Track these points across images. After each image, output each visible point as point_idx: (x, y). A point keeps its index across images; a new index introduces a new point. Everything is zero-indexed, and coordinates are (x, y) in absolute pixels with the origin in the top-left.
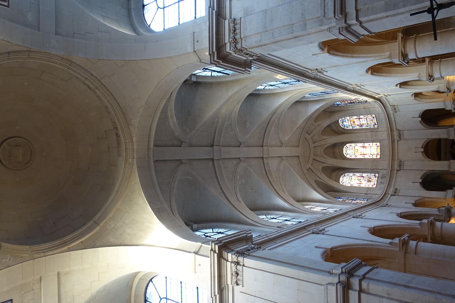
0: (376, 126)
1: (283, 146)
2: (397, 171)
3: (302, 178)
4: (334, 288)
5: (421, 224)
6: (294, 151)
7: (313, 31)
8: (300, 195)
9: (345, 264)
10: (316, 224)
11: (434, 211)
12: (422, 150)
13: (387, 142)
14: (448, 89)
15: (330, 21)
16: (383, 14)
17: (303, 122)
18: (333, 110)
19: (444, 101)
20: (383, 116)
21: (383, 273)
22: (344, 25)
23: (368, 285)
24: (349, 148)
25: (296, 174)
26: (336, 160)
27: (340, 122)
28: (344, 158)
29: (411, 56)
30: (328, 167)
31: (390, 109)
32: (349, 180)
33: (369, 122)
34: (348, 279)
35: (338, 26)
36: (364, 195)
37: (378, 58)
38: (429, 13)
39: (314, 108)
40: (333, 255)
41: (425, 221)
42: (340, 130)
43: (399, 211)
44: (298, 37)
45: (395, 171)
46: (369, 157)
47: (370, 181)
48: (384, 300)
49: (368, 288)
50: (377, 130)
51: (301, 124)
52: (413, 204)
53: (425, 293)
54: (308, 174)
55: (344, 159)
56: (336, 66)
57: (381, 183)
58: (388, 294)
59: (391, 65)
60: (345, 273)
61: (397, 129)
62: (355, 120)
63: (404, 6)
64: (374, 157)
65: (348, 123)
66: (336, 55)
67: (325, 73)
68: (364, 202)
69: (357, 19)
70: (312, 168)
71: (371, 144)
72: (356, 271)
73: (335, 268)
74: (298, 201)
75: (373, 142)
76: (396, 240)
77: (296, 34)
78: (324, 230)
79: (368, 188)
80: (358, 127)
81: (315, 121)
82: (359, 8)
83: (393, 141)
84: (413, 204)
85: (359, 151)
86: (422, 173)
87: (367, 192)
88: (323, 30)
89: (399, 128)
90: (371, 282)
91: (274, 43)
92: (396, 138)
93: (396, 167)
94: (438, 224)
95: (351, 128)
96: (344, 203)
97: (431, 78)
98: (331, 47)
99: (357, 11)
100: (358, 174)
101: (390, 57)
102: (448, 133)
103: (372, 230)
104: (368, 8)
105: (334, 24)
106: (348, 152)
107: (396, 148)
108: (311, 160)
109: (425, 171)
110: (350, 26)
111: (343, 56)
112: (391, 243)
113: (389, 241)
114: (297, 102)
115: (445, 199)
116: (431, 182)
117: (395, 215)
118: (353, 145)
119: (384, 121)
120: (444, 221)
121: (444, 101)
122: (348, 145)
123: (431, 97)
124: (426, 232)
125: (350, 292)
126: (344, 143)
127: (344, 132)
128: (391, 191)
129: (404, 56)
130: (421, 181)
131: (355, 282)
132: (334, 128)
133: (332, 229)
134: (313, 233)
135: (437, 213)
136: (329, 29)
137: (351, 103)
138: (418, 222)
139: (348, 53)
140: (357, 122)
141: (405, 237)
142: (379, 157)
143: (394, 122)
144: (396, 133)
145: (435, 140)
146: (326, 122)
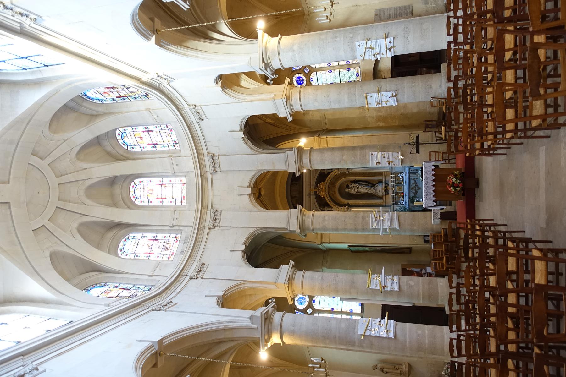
2: (210, 229)
12: (249, 191)
13: (194, 176)
19: (273, 99)
24: (138, 187)
26: (116, 210)
28: (130, 204)
29: (502, 234)
31: (188, 111)
32: (135, 246)
33: (165, 139)
36: (146, 277)
42: (121, 152)
45: (206, 229)
46: (170, 204)
47: (167, 249)
50: (178, 155)
55: (129, 208)
61: (208, 153)
64: (179, 204)
71: (173, 179)
75: (174, 174)
78: (37, 369)
83: (203, 176)
89: (212, 150)
92: (209, 168)
93: (208, 222)
95: (137, 149)
100: (150, 235)
102: (287, 160)
106: (138, 194)
108: (50, 211)
109: (252, 230)
112: (251, 318)
116: (263, 251)
118: (145, 180)
122: (137, 181)
127: (125, 156)
128: (191, 271)
130: (243, 248)
144: (207, 160)
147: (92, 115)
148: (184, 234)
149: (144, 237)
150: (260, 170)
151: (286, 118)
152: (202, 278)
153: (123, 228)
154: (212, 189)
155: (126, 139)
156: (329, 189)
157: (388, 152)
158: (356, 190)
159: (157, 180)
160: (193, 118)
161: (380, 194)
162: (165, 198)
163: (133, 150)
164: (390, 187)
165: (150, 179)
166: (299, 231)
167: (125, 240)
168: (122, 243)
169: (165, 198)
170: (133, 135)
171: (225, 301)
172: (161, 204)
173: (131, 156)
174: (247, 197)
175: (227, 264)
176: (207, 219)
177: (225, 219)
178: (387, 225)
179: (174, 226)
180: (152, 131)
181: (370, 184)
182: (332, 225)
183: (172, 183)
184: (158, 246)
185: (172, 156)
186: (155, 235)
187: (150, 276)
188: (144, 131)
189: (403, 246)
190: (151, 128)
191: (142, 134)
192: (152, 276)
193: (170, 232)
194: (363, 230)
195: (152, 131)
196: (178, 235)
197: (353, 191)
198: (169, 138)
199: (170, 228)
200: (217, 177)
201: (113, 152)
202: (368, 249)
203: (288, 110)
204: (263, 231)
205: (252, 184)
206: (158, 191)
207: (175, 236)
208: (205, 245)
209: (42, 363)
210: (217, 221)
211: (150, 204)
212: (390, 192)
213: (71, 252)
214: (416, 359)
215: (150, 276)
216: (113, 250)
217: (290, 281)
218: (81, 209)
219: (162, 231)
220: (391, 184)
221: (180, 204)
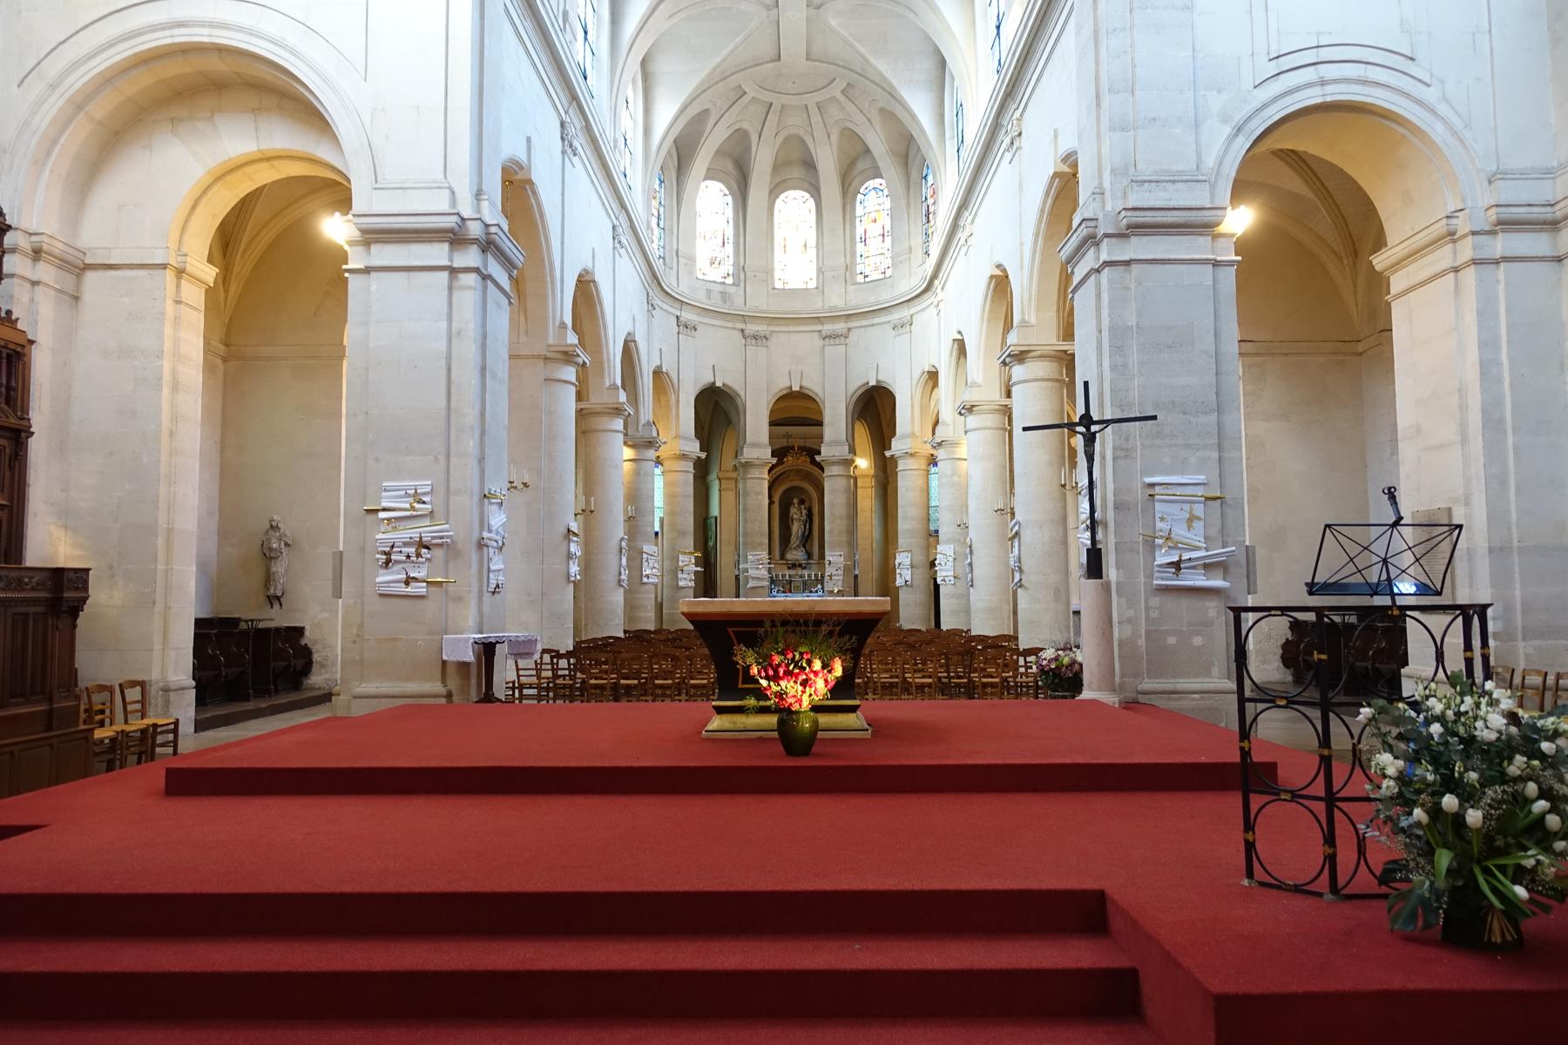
0: (860, 279)
1: (813, 11)
3: (714, 70)
4: (444, 206)
5: (614, 387)
6: (793, 48)
7: (1105, 149)
8: (663, 67)
9: (506, 228)
10: (588, 128)
11: (647, 412)
12: (796, 388)
13: (817, 306)
14: (940, 444)
15: (1120, 194)
16: (1105, 323)
17: (881, 74)
18: (910, 159)
19: (912, 435)
20: (885, 297)
21: (501, 318)
22: (1100, 232)
23: (470, 288)
25: (725, 53)
26: (769, 170)
27: (878, 181)
28: (775, 191)
29: (1018, 372)
30: (749, 147)
31: (904, 313)
32: (711, 201)
34: (475, 241)
35: (1100, 216)
37: (1026, 296)
38: (1082, 417)
39: (920, 106)
40: (517, 188)
41: (623, 397)
42: (854, 184)
43: (640, 338)
44: (1098, 105)
45: (742, 326)
47: (712, 263)
48: (444, 324)
49: (462, 288)
51: (875, 69)
52: (660, 367)
53: (477, 408)
54: (727, 86)
56: (1021, 189)
57: (709, 292)
58: (459, 333)
59: (1008, 325)
60: (488, 234)
62: (879, 225)
63: (1113, 368)
65: (874, 201)
66: (1047, 194)
67: (1008, 156)
68: (654, 249)
69: (1107, 264)
70: (746, 99)
72: (495, 257)
73: (492, 204)
74: (644, 63)
75: (820, 271)
76: (572, 339)
77: (1106, 100)
79: (692, 259)
80: (859, 232)
81: (882, 111)
82: (1134, 267)
84: (660, 367)
87: (681, 256)
88: (1100, 176)
90: (479, 293)
91: (1096, 32)
92: (828, 328)
93: (752, 328)
94: (619, 424)
95: (859, 210)
96: (650, 195)
97: (968, 409)
98: (1065, 186)
99: (1127, 263)
100: (730, 232)
101: (1025, 324)
102: (836, 443)
103: (520, 176)
104: (1127, 288)
105: (1109, 207)
107: (801, 328)
108: (767, 97)
109: (742, 394)
110: (1097, 244)
111: (1042, 211)
112: (563, 325)
113: (568, 320)
114: (943, 63)
115: (677, 436)
116: (716, 410)
117: (629, 328)
119: (872, 299)
120: (626, 435)
121: (912, 435)
122: (811, 203)
123: (924, 408)
124: (596, 399)
125: (446, 246)
126: (815, 191)
127: (848, 191)
128: (688, 316)
129: (1021, 357)
131: (471, 257)
132: (862, 165)
133: (581, 175)
134: (562, 125)
135: (643, 421)
136: (1100, 193)
137: (928, 215)
138: (619, 382)
139: (1050, 224)
141: (583, 357)
143: (869, 322)
144: (840, 327)
145: (821, 413)
146: (877, 141)
148: (732, 290)
153: (739, 179)
156: (798, 472)
157: (154, 745)
160: (896, 316)
161: (789, 556)
164: (800, 572)
171: (658, 373)
175: (700, 362)
176: (755, 328)
177: (756, 353)
178: (752, 572)
181: (806, 539)
182: (749, 503)
190: (888, 239)
191: (879, 225)
193: (736, 265)
194: (745, 544)
197: (794, 511)
201: (856, 172)
202: (711, 544)
203: (898, 454)
212: (792, 572)
216: (710, 176)
217: (684, 457)
220: (806, 573)
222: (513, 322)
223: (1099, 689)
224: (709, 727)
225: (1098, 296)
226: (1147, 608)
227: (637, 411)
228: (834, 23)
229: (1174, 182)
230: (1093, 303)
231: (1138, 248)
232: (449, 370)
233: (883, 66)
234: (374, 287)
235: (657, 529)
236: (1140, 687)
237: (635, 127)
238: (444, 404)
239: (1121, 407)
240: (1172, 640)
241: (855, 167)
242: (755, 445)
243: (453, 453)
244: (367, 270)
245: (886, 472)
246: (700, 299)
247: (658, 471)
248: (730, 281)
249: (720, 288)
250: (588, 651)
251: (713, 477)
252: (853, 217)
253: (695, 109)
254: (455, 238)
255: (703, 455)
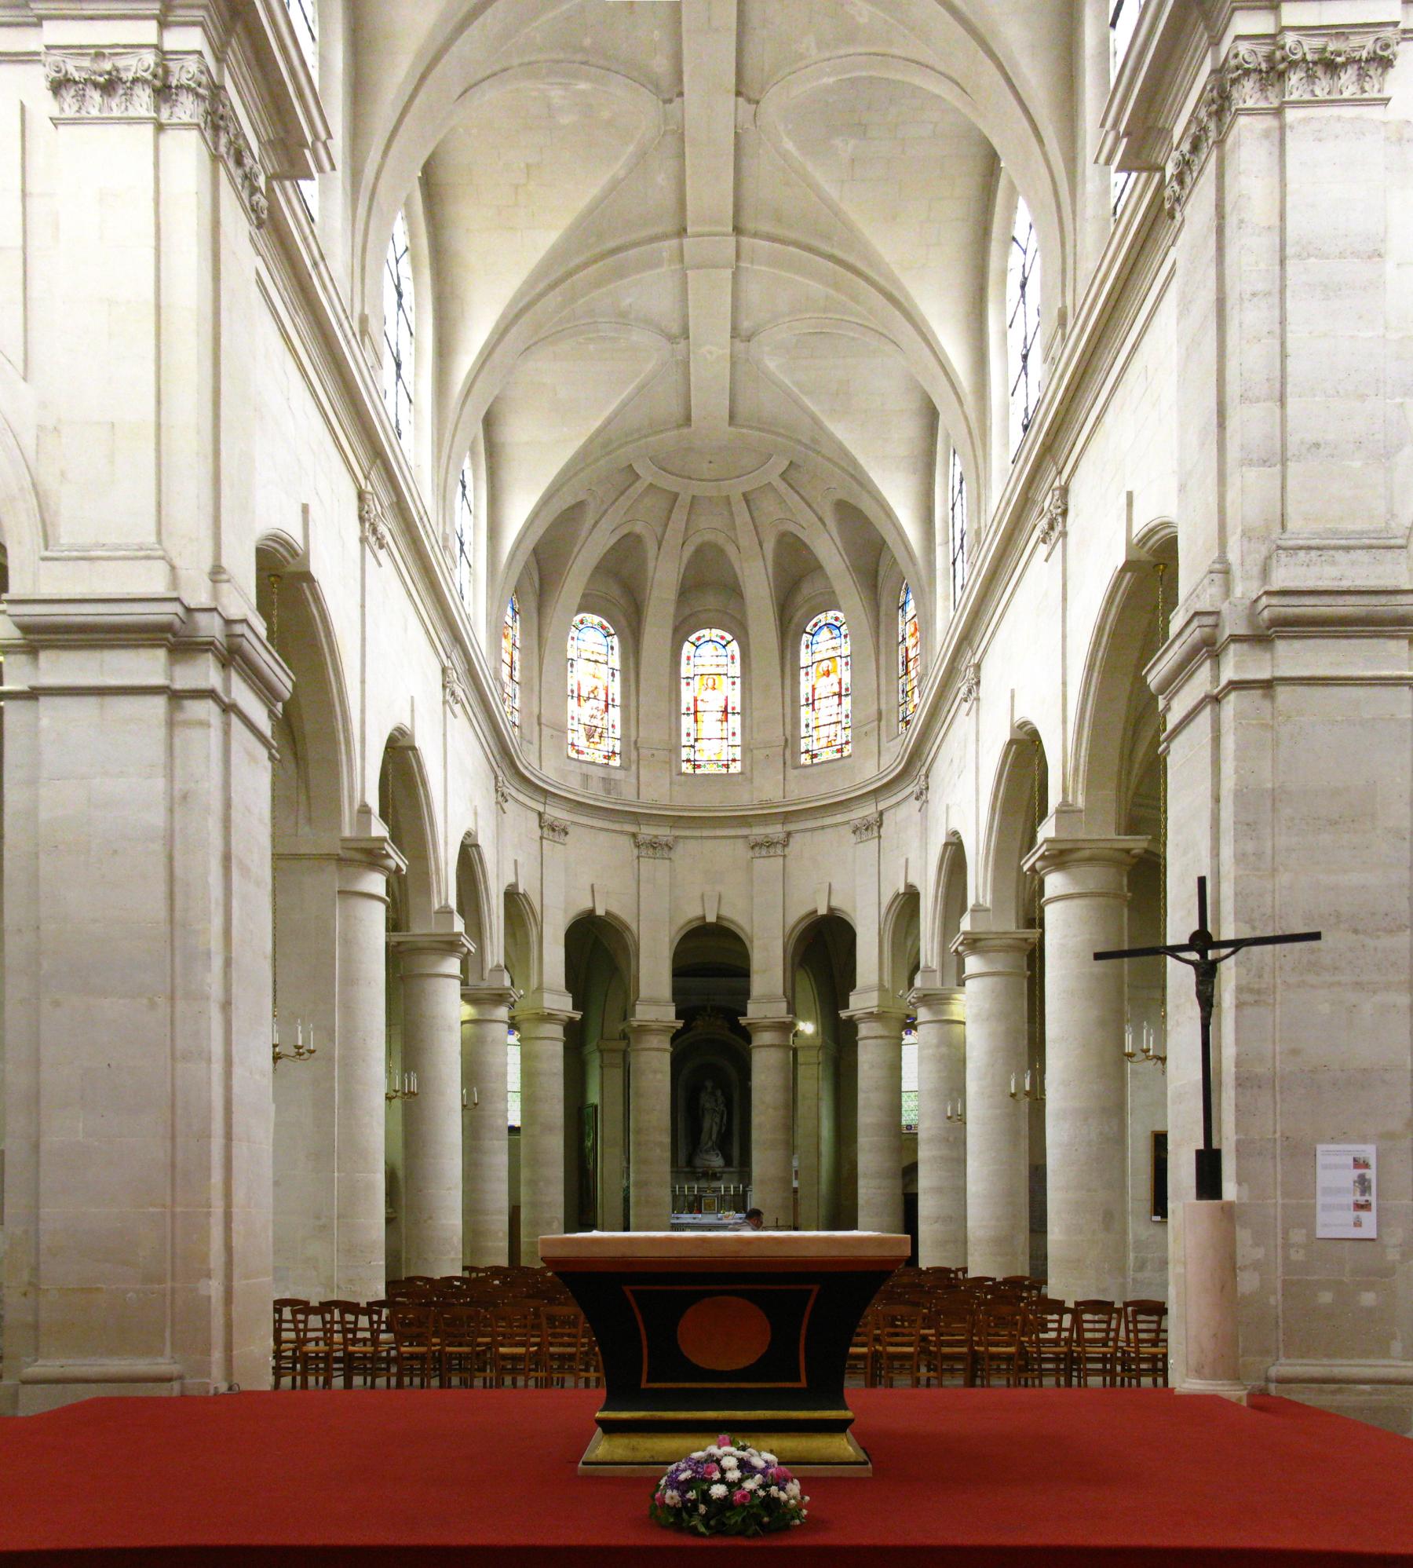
0: (805, 759)
2: (634, 835)
3: (591, 440)
4: (160, 588)
5: (446, 912)
12: (711, 918)
13: (744, 799)
16: (1228, 784)
18: (879, 571)
20: (841, 786)
21: (255, 779)
24: (721, 651)
28: (681, 631)
32: (591, 650)
35: (1225, 607)
38: (1194, 937)
39: (898, 497)
40: (283, 578)
41: (459, 925)
42: (798, 616)
43: (485, 841)
47: (590, 736)
49: (187, 724)
50: (789, 763)
51: (831, 437)
58: (185, 797)
62: (834, 678)
63: (1240, 858)
64: (685, 753)
65: (827, 651)
69: (1235, 685)
70: (640, 486)
71: (738, 740)
72: (246, 678)
75: (746, 748)
80: (805, 689)
83: (744, 821)
85: (709, 695)
86: (625, 914)
89: (796, 843)
93: (647, 831)
94: (453, 965)
95: (805, 658)
96: (497, 631)
98: (1152, 569)
100: (616, 689)
102: (770, 999)
106: (707, 650)
108: (671, 483)
109: (634, 927)
112: (365, 810)
113: (373, 801)
116: (596, 947)
117: (468, 825)
118: (735, 669)
119: (823, 789)
120: (464, 983)
122: (734, 647)
124: (420, 928)
125: (161, 654)
126: (741, 633)
127: (789, 631)
128: (555, 813)
130: (600, 912)
131: (206, 673)
132: (807, 590)
138: (453, 903)
140: (826, 686)
142: (687, 768)
146: (830, 552)
147: (875, 575)
148: (619, 775)
149: (613, 675)
150: (752, 942)
151: (847, 1007)
152: (541, 838)
153: (629, 626)
154: (715, 838)
155: (825, 633)
158: (708, 1105)
159: (735, 701)
162: (696, 721)
163: (803, 647)
165: (738, 681)
166: (635, 1024)
167: (603, 628)
168: (596, 619)
169: (696, 721)
170: (832, 654)
171: (512, 896)
172: (684, 710)
173: (789, 643)
174: (698, 912)
176: (655, 829)
179: (637, 749)
180: (840, 704)
183: (730, 737)
184: (595, 712)
185: (786, 746)
186: (618, 702)
187: (539, 718)
188: (840, 683)
189: (599, 1211)
190: (847, 702)
191: (834, 678)
192: (540, 724)
195: (840, 704)
196: (618, 757)
197: (706, 1101)
198: (823, 742)
199: (633, 739)
200: (741, 849)
202: (589, 1144)
203: (859, 1014)
204: (632, 949)
205: (726, 924)
206: (712, 702)
207: (617, 750)
208: (601, 829)
209: (391, 555)
210: (651, 852)
211: (683, 682)
212: (704, 1184)
213: (584, 534)
214: (403, 1230)
215: (539, 718)
218: (673, 536)
219: (625, 720)
221: (684, 757)
222: (280, 800)
223: (1214, 1376)
224: (588, 1456)
225: (1216, 740)
226: (1287, 1246)
227: (481, 948)
228: (772, 364)
229: (1347, 549)
230: (1207, 753)
231: (1295, 658)
232: (171, 858)
233: (842, 431)
234: (45, 722)
235: (515, 1119)
236: (1273, 1372)
237: (476, 538)
238: (162, 914)
239: (1250, 921)
240: (1326, 1297)
241: (796, 596)
242: (654, 1002)
243: (179, 993)
244: (33, 694)
245: (841, 1039)
246: (572, 786)
247: (513, 1039)
248: (616, 762)
249: (601, 773)
250: (412, 1299)
251: (591, 1047)
252: (796, 668)
253: (566, 500)
254: (177, 639)
255: (578, 1016)
